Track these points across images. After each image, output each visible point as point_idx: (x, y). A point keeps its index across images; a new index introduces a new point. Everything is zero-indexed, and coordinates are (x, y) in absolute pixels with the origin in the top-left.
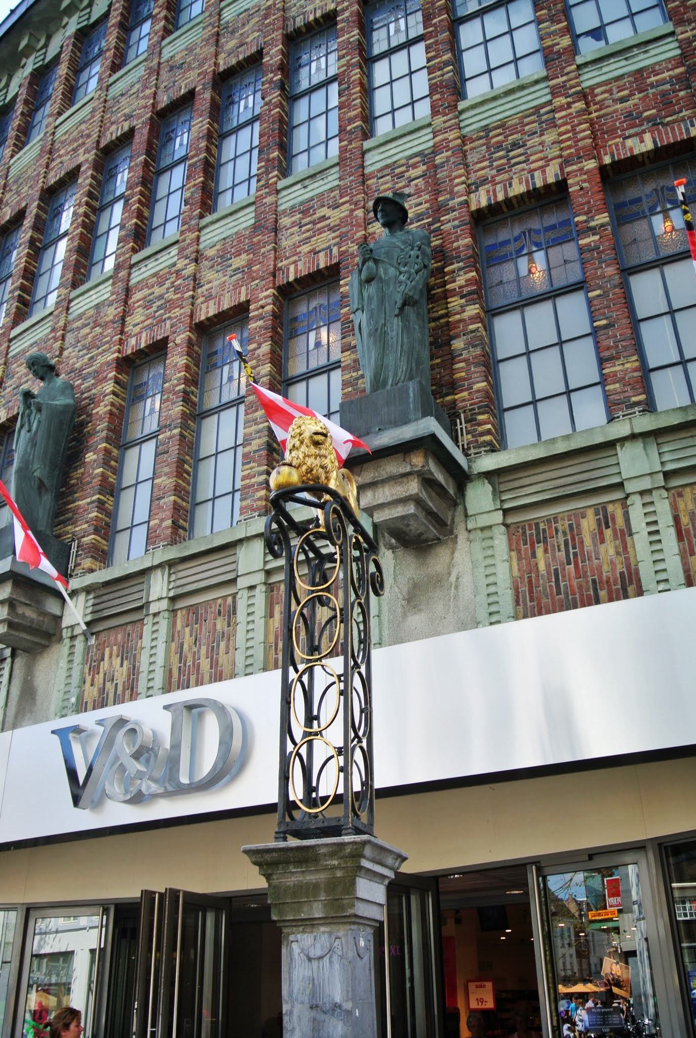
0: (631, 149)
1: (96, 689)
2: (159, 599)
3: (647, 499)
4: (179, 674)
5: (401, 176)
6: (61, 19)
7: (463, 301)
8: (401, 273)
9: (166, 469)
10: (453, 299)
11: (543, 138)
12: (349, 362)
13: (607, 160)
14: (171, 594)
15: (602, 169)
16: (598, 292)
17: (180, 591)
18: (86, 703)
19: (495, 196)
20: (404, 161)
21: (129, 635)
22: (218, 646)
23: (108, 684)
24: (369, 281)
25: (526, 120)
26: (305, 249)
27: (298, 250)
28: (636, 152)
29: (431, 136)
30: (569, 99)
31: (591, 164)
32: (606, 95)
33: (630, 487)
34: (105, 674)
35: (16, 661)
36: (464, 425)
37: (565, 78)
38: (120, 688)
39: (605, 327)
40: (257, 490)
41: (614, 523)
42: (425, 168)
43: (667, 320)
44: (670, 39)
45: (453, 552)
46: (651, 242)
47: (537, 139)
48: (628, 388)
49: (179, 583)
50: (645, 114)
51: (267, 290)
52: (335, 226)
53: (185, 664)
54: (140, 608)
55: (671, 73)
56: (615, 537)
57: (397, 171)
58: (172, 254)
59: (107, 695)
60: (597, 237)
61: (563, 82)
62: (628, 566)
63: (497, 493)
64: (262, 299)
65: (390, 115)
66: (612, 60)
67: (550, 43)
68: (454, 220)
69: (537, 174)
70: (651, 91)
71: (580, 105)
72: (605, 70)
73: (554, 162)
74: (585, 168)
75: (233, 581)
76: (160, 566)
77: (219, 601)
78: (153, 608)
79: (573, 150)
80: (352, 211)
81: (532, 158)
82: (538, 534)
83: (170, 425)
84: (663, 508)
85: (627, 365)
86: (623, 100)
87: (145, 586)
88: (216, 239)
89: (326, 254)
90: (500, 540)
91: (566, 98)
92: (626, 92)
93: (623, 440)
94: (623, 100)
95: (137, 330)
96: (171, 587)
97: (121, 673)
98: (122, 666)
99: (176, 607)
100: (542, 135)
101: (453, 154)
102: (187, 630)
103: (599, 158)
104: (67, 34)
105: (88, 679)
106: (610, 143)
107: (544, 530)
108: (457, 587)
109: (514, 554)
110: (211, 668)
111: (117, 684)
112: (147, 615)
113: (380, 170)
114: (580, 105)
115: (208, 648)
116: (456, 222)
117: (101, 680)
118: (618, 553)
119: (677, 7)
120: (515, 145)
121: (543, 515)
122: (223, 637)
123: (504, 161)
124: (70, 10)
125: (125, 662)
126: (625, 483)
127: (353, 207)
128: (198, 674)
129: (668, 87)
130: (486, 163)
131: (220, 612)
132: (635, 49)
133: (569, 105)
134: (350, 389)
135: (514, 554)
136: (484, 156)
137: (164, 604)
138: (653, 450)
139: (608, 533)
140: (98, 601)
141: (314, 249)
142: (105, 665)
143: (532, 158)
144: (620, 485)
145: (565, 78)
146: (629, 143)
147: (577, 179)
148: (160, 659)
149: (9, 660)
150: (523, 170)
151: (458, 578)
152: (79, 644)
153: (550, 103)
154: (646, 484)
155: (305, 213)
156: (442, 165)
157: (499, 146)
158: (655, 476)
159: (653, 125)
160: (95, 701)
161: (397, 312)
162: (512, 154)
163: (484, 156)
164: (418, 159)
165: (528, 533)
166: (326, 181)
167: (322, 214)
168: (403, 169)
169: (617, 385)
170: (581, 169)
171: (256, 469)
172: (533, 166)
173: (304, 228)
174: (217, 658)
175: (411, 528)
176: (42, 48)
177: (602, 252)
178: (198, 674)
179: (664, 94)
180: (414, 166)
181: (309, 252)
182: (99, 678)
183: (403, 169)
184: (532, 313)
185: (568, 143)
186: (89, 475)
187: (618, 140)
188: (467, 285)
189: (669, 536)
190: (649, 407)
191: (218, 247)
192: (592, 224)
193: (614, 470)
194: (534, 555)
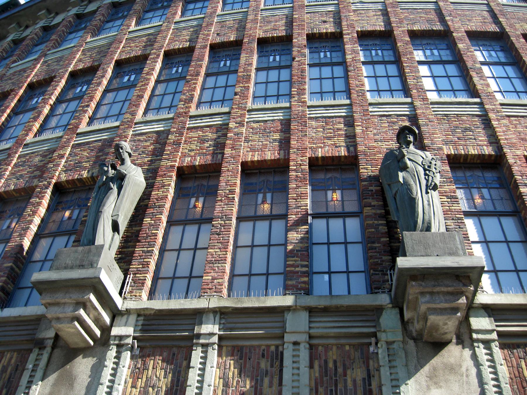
6: (68, 7)
12: (370, 214)
21: (174, 354)
22: (262, 380)
35: (55, 351)
36: (130, 280)
43: (326, 247)
46: (325, 203)
65: (225, 99)
104: (69, 14)
124: (74, 5)
131: (263, 356)
140: (147, 323)
149: (49, 349)
174: (261, 390)
175: (446, 327)
176: (21, 31)
184: (259, 224)
190: (308, 292)
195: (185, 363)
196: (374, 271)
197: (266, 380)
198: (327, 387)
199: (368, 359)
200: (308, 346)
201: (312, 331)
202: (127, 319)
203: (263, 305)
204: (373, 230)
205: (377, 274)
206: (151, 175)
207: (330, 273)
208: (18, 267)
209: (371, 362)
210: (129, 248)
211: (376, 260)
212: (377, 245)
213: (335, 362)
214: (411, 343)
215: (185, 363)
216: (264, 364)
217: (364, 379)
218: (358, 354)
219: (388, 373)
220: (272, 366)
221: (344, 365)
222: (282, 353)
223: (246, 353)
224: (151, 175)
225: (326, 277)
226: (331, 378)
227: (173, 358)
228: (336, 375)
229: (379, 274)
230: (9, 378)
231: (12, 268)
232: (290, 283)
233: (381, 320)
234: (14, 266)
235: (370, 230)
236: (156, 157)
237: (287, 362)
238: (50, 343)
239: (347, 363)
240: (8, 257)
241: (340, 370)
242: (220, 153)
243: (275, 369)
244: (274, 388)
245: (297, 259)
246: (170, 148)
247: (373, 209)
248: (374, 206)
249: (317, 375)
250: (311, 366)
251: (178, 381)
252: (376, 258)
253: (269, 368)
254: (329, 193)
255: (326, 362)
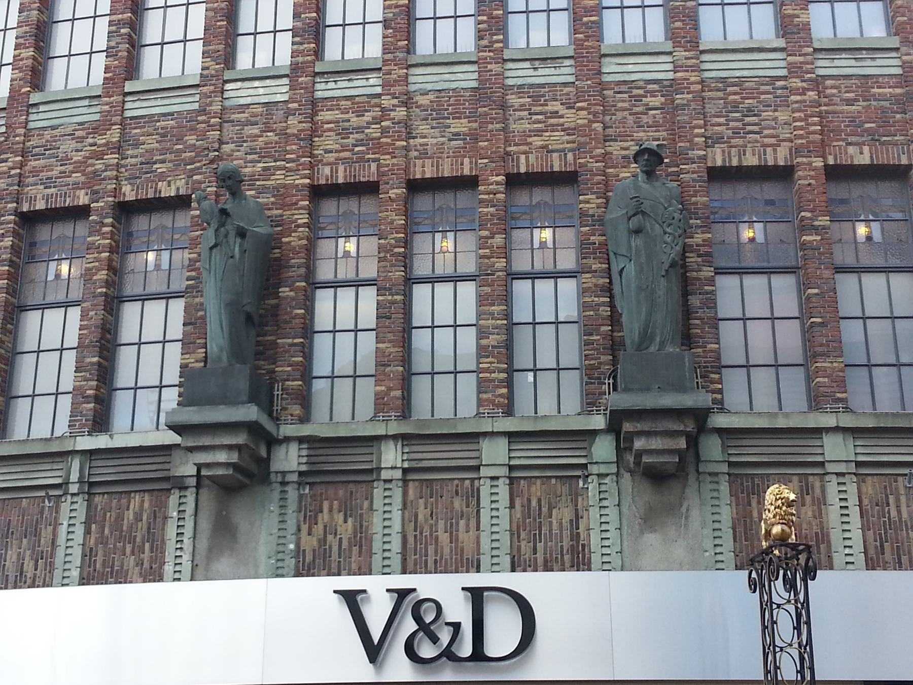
0: (852, 157)
1: (315, 539)
2: (392, 468)
3: (841, 480)
4: (416, 542)
5: (638, 98)
7: (700, 259)
8: (665, 233)
9: (390, 336)
10: (691, 255)
11: (776, 114)
12: (590, 285)
13: (831, 161)
14: (406, 465)
15: (826, 166)
16: (816, 291)
17: (414, 464)
18: (304, 551)
19: (730, 160)
20: (641, 83)
21: (352, 493)
22: (457, 524)
23: (330, 538)
24: (638, 231)
25: (763, 88)
26: (537, 141)
27: (529, 140)
28: (856, 162)
29: (670, 67)
30: (804, 84)
31: (818, 163)
32: (835, 91)
33: (830, 468)
34: (325, 527)
35: (201, 491)
37: (801, 59)
38: (345, 544)
39: (822, 324)
40: (498, 387)
41: (813, 492)
42: (663, 99)
44: (894, 54)
45: (684, 488)
47: (771, 113)
48: (834, 384)
49: (413, 456)
50: (867, 125)
51: (497, 175)
52: (569, 129)
53: (421, 533)
54: (371, 471)
55: (891, 90)
56: (813, 504)
57: (635, 92)
58: (372, 82)
59: (330, 547)
60: (819, 238)
61: (801, 63)
62: (822, 529)
63: (725, 447)
64: (492, 184)
66: (843, 56)
67: (791, 12)
68: (693, 173)
69: (769, 150)
70: (873, 103)
71: (812, 95)
72: (837, 63)
73: (785, 143)
74: (814, 164)
75: (477, 468)
76: (395, 437)
77: (456, 482)
78: (385, 475)
79: (804, 141)
80: (590, 121)
81: (766, 132)
82: (753, 487)
83: (390, 289)
84: (852, 488)
85: (835, 365)
86: (850, 102)
87: (374, 450)
88: (429, 87)
89: (560, 156)
90: (724, 487)
91: (802, 81)
92: (852, 95)
93: (828, 430)
94: (850, 102)
95: (331, 157)
96: (405, 458)
97: (346, 529)
98: (345, 522)
99: (408, 478)
100: (775, 111)
101: (694, 99)
102: (422, 501)
103: (824, 157)
105: (305, 528)
106: (835, 144)
107: (758, 485)
108: (687, 518)
109: (733, 498)
110: (451, 543)
111: (341, 539)
112: (378, 480)
113: (619, 83)
114: (812, 95)
115: (446, 523)
116: (695, 176)
117: (321, 531)
118: (815, 517)
119: (904, 23)
120: (750, 112)
121: (759, 472)
122: (462, 516)
123: (739, 124)
125: (350, 520)
126: (826, 464)
127: (591, 117)
128: (437, 544)
129: (886, 104)
130: (722, 120)
132: (864, 52)
133: (804, 92)
134: (592, 313)
135: (733, 498)
136: (721, 112)
137: (398, 474)
138: (850, 442)
139: (808, 499)
140: (312, 452)
141: (547, 146)
142: (324, 517)
143: (766, 132)
144: (822, 464)
145: (801, 59)
146: (851, 150)
147: (806, 173)
148: (397, 526)
150: (757, 142)
151: (688, 510)
152: (292, 493)
153: (784, 78)
154: (842, 468)
155: (536, 98)
156: (682, 107)
157: (735, 107)
158: (849, 464)
159: (872, 139)
160: (314, 551)
161: (663, 273)
162: (747, 119)
163: (721, 112)
164: (656, 87)
165: (745, 484)
166: (558, 72)
167: (555, 109)
168: (641, 92)
169: (826, 380)
170: (810, 164)
171: (495, 365)
172: (766, 140)
173: (535, 117)
177: (823, 254)
178: (437, 544)
179: (883, 110)
180: (653, 93)
181: (542, 147)
182: (319, 529)
183: (641, 92)
185: (801, 132)
186: (287, 313)
187: (841, 143)
188: (704, 245)
189: (855, 512)
191: (431, 97)
192: (816, 223)
193: (819, 451)
194: (749, 504)
195: (366, 504)
196: (589, 378)
197: (462, 523)
198: (530, 531)
199: (577, 495)
200: (507, 481)
201: (511, 463)
202: (287, 448)
203: (453, 432)
204: (592, 313)
205: (592, 383)
206: (272, 199)
207: (535, 370)
208: (104, 359)
209: (580, 499)
210: (265, 335)
211: (592, 362)
212: (595, 338)
213: (539, 500)
214: (627, 476)
215: (366, 504)
216: (458, 504)
217: (571, 521)
218: (565, 489)
219: (598, 516)
220: (468, 506)
221: (550, 504)
222: (478, 490)
223: (437, 490)
224: (272, 199)
225: (530, 375)
226: (535, 520)
227: (351, 498)
228: (540, 515)
229: (594, 383)
230: (149, 528)
231: (99, 364)
232: (485, 396)
233: (593, 449)
234: (101, 360)
235: (588, 313)
236: (275, 161)
237: (485, 501)
238: (193, 482)
239: (552, 501)
240: (87, 347)
241: (545, 510)
242: (374, 160)
243: (472, 510)
244: (471, 532)
245: (493, 360)
246: (294, 147)
247: (594, 276)
248: (596, 271)
249: (519, 516)
250: (512, 506)
251: (361, 526)
252: (592, 359)
253: (465, 509)
254: (536, 232)
255: (529, 501)
